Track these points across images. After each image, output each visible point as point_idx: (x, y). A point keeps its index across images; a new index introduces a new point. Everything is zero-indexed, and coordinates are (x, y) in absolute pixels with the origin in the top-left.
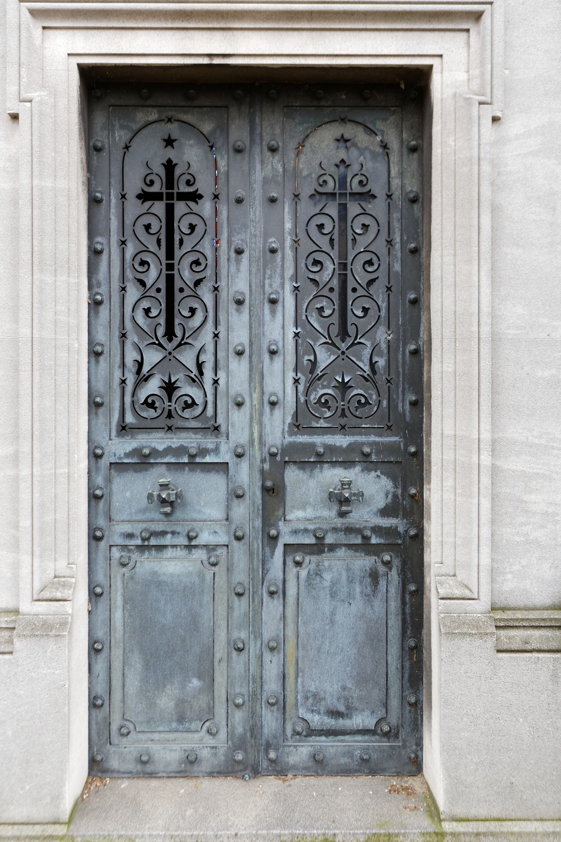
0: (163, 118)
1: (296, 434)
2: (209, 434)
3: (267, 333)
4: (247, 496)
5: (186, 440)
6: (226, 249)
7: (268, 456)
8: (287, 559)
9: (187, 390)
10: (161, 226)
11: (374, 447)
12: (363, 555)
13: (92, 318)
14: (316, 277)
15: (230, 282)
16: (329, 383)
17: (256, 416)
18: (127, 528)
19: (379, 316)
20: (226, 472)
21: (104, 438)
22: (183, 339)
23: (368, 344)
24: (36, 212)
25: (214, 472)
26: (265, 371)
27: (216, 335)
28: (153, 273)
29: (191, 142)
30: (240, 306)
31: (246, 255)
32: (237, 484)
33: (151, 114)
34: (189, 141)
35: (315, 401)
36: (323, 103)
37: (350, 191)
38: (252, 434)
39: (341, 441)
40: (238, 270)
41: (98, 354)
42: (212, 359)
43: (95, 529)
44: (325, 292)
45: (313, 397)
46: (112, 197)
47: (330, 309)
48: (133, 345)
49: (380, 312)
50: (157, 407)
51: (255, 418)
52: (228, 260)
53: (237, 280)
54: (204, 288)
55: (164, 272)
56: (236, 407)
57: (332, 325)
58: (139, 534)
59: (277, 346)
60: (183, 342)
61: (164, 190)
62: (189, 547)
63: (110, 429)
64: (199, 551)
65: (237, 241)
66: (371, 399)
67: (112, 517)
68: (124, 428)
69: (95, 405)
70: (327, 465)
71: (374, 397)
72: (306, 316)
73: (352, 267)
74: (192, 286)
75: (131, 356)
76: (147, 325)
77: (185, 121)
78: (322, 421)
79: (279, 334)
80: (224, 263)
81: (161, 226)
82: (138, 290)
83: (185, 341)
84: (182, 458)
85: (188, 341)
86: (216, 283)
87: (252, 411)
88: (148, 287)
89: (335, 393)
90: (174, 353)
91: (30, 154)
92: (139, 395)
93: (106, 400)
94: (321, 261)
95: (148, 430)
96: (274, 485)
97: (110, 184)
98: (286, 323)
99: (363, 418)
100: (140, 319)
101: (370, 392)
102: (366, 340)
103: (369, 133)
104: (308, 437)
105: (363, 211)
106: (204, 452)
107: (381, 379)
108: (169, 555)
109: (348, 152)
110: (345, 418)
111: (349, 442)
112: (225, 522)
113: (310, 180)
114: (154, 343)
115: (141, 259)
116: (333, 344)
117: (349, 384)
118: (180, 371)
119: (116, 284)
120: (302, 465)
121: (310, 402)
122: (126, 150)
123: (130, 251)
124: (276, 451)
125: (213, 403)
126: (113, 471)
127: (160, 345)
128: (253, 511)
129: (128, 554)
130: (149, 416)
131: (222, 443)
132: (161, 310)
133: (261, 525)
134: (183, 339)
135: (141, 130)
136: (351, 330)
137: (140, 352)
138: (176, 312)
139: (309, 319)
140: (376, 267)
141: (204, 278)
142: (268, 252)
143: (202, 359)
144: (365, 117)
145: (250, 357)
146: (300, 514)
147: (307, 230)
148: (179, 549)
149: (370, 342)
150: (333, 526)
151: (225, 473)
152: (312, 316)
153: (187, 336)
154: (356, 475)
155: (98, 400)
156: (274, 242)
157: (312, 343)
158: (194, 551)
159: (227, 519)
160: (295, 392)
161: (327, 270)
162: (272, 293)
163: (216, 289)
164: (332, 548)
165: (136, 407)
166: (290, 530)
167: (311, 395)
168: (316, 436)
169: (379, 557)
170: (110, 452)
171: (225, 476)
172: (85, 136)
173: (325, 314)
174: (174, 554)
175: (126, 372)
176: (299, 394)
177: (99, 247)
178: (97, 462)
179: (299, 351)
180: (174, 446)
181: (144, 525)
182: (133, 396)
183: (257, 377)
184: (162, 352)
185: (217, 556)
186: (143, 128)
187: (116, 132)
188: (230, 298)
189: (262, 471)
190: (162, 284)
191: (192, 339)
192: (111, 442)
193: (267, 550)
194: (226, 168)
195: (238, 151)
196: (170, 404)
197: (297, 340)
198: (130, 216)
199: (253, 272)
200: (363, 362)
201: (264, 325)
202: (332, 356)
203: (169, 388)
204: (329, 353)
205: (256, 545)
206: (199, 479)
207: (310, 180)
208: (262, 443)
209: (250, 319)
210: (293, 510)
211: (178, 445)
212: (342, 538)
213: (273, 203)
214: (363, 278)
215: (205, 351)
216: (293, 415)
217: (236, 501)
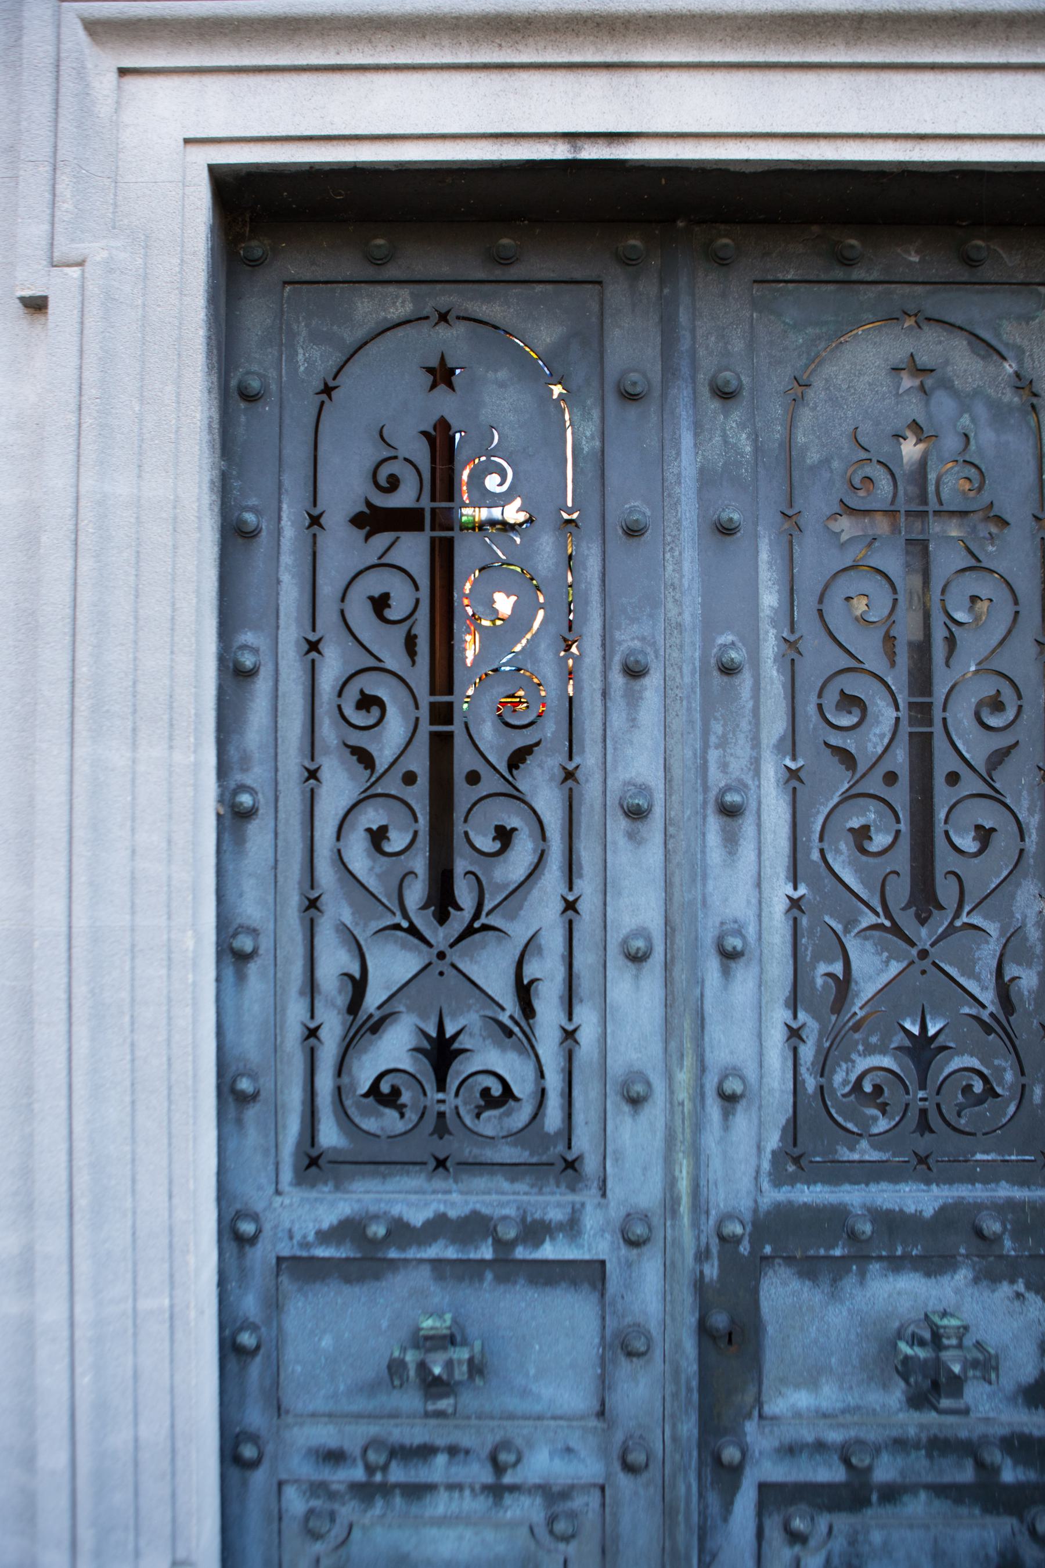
0: (425, 313)
1: (792, 1180)
2: (552, 1181)
3: (715, 900)
4: (658, 1354)
5: (487, 1198)
6: (598, 662)
7: (714, 1242)
8: (768, 1523)
9: (488, 1058)
10: (417, 601)
11: (1010, 1216)
12: (977, 1511)
13: (227, 856)
14: (849, 743)
15: (609, 758)
16: (886, 1038)
17: (684, 1134)
18: (325, 1435)
19: (1022, 851)
20: (600, 1287)
21: (260, 1188)
22: (477, 916)
23: (992, 928)
24: (86, 565)
25: (564, 1285)
26: (708, 1008)
27: (570, 906)
28: (395, 730)
29: (502, 374)
30: (639, 825)
31: (652, 682)
32: (629, 1320)
33: (394, 303)
34: (496, 371)
35: (847, 1089)
36: (857, 274)
37: (937, 508)
38: (671, 1183)
39: (919, 1199)
40: (633, 722)
41: (242, 958)
42: (560, 973)
43: (237, 1436)
44: (874, 784)
45: (841, 1078)
46: (285, 522)
47: (887, 832)
48: (337, 930)
49: (1022, 839)
50: (404, 1106)
51: (680, 1137)
52: (605, 694)
53: (629, 752)
54: (537, 771)
55: (426, 728)
56: (626, 1108)
57: (893, 876)
58: (357, 1452)
59: (744, 938)
60: (477, 925)
61: (426, 503)
62: (497, 1491)
63: (277, 1165)
64: (522, 1498)
65: (627, 639)
66: (1001, 1081)
67: (285, 1402)
68: (314, 1162)
69: (234, 1097)
70: (877, 1266)
71: (1009, 1076)
72: (822, 852)
73: (947, 714)
74: (503, 767)
75: (334, 962)
76: (379, 876)
77: (486, 319)
78: (864, 1144)
79: (749, 902)
80: (592, 702)
81: (417, 601)
82: (353, 777)
83: (483, 920)
84: (476, 1248)
85: (492, 921)
86: (571, 758)
87: (672, 1120)
88: (380, 768)
89: (900, 1065)
90: (453, 956)
91: (73, 406)
92: (355, 1070)
93: (266, 1084)
94: (862, 697)
95: (382, 1168)
96: (732, 1321)
97: (280, 488)
98: (767, 871)
99: (979, 1135)
100: (359, 857)
101: (996, 1062)
102: (986, 917)
103: (982, 353)
104: (827, 1188)
105: (973, 563)
106: (536, 1231)
107: (1026, 1026)
108: (441, 1510)
109: (927, 404)
110: (927, 1135)
111: (941, 1202)
112: (593, 1423)
113: (827, 475)
114: (397, 927)
115: (362, 692)
116: (896, 930)
117: (941, 1041)
118: (470, 1007)
119: (292, 762)
120: (809, 1268)
121: (833, 1091)
122: (324, 397)
123: (332, 668)
124: (739, 1230)
125: (562, 1094)
126: (284, 1279)
127: (413, 930)
128: (675, 1395)
129: (328, 1506)
130: (382, 1129)
131: (589, 1208)
132: (416, 833)
133: (696, 1432)
134: (477, 916)
135: (366, 343)
136: (946, 891)
137: (357, 952)
138: (458, 840)
139: (830, 861)
140: (1010, 714)
141: (537, 744)
142: (716, 673)
143: (530, 971)
144: (969, 307)
145: (667, 967)
146: (802, 1399)
147: (820, 611)
148: (467, 1493)
149: (998, 925)
150: (895, 1433)
151: (594, 1287)
152: (838, 851)
153: (487, 907)
154: (957, 1291)
155: (245, 1085)
156: (733, 643)
157: (838, 928)
158: (508, 1499)
159: (601, 1414)
160: (790, 1063)
161: (878, 722)
162: (728, 789)
163: (569, 775)
164: (891, 1494)
165: (348, 1103)
166: (777, 1444)
167: (833, 1072)
168: (847, 1187)
169: (1021, 1519)
170: (276, 1227)
171: (594, 1297)
172: (219, 362)
173: (874, 847)
174: (454, 1507)
175: (319, 1005)
176: (803, 1070)
177: (248, 661)
178: (241, 1255)
179: (801, 949)
180: (453, 1214)
181: (373, 1429)
182: (339, 1073)
183: (687, 1025)
184: (420, 952)
185: (572, 1515)
186: (373, 339)
187: (301, 351)
188: (612, 800)
189: (700, 1285)
190: (419, 762)
191: (504, 916)
192: (278, 1200)
193: (713, 1499)
194: (597, 443)
195: (629, 397)
196: (441, 1096)
197: (795, 919)
198: (333, 573)
199: (674, 727)
200: (977, 978)
201: (705, 877)
202: (893, 963)
203: (441, 1052)
204: (886, 954)
205: (682, 1489)
206: (523, 1305)
207: (827, 475)
208: (699, 1206)
209: (667, 859)
210: (784, 1390)
211: (466, 1210)
212: (921, 1467)
213: (729, 538)
214: (976, 747)
215: (540, 950)
216: (784, 1130)
217: (625, 1366)
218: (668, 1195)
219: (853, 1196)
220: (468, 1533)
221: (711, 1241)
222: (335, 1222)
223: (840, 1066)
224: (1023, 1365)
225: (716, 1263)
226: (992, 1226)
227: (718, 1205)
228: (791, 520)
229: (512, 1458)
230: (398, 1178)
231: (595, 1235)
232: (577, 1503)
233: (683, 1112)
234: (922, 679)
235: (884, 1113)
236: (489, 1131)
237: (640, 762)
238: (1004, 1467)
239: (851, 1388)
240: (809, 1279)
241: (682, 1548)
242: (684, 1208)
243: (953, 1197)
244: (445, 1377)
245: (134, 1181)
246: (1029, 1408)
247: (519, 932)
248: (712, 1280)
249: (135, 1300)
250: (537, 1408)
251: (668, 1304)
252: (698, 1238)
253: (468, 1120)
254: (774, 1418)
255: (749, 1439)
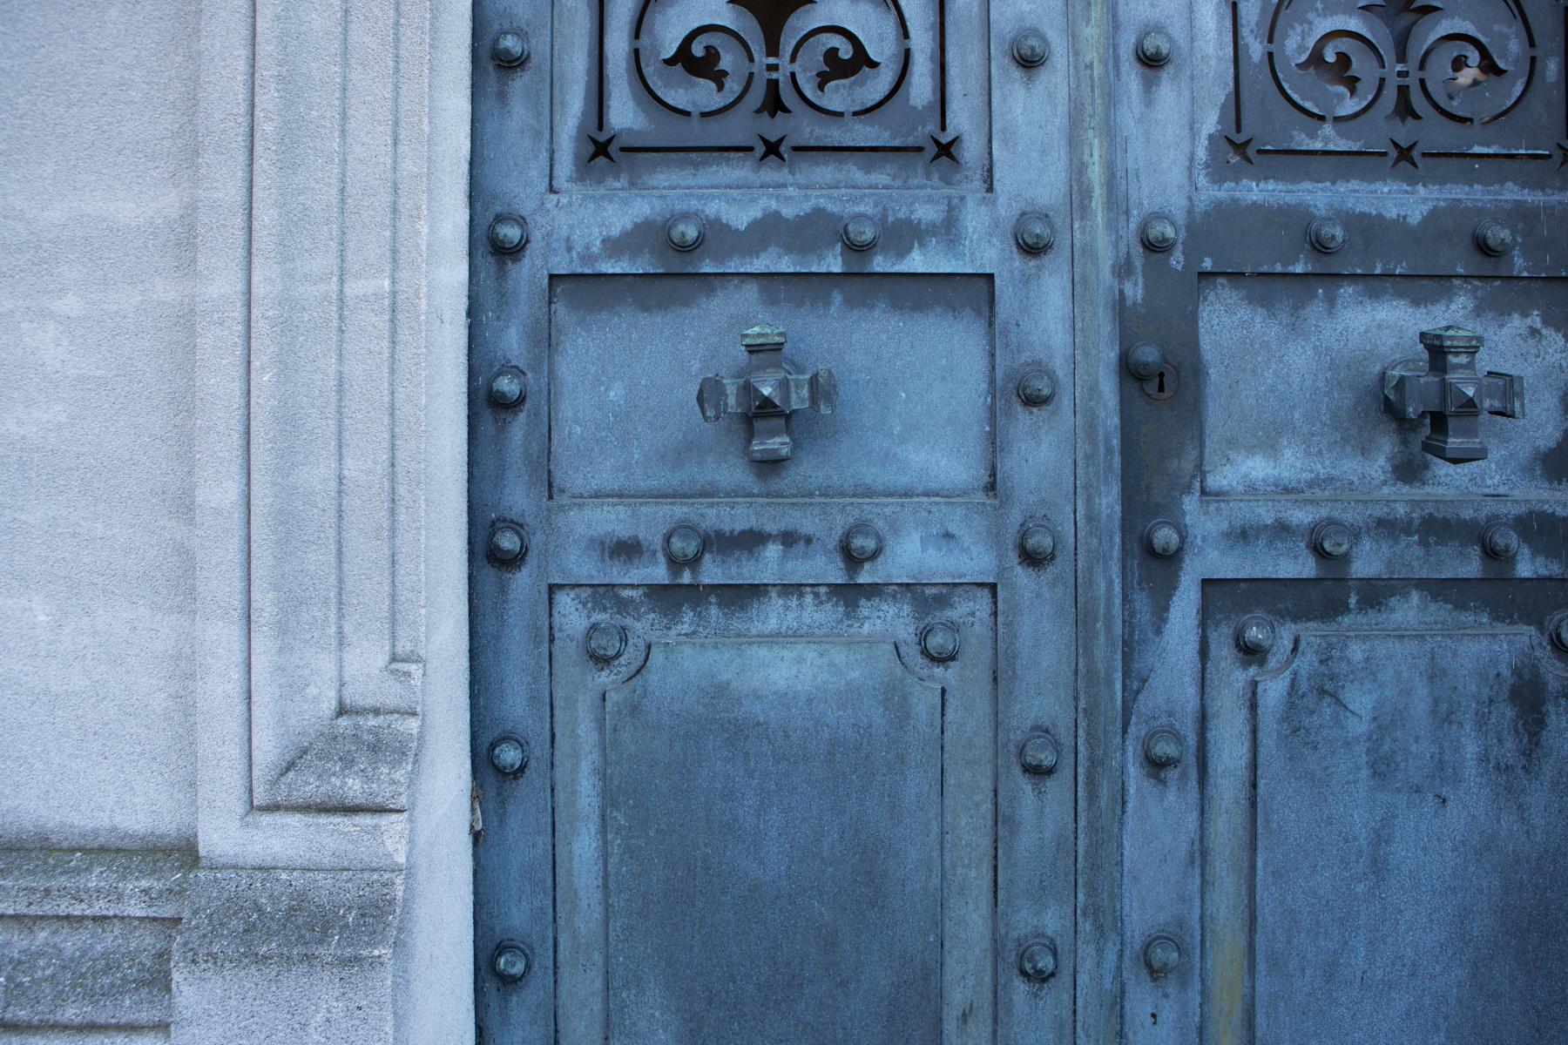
2: (921, 171)
4: (1066, 403)
5: (835, 192)
7: (1137, 250)
8: (1213, 636)
18: (613, 521)
32: (1026, 356)
38: (1078, 170)
39: (1403, 201)
43: (493, 523)
45: (1296, 44)
50: (724, 73)
51: (1089, 110)
56: (1017, 73)
58: (658, 543)
62: (849, 594)
64: (885, 607)
84: (821, 258)
92: (658, 28)
93: (539, 46)
95: (694, 155)
106: (904, 235)
108: (773, 624)
110: (1410, 121)
112: (980, 497)
120: (1262, 284)
124: (1170, 232)
126: (560, 308)
128: (1090, 457)
129: (618, 620)
131: (970, 204)
133: (1118, 508)
146: (1257, 468)
148: (809, 599)
150: (1379, 512)
151: (979, 313)
159: (991, 487)
160: (1228, 23)
164: (1376, 593)
165: (648, 71)
166: (1225, 526)
167: (1286, 35)
168: (1307, 185)
170: (549, 235)
171: (979, 327)
174: (791, 620)
176: (1245, 32)
178: (502, 274)
180: (788, 212)
181: (680, 511)
182: (637, 33)
185: (953, 627)
189: (1120, 307)
193: (1141, 601)
196: (772, 60)
205: (1103, 586)
206: (884, 337)
208: (1117, 204)
210: (1232, 455)
211: (807, 207)
212: (1413, 558)
217: (1024, 419)
218: (1075, 188)
220: (810, 654)
221: (1133, 251)
222: (629, 226)
223: (1293, 28)
224: (1540, 423)
225: (1140, 281)
227: (1141, 203)
229: (870, 544)
230: (714, 168)
231: (979, 239)
232: (960, 610)
233: (1091, 77)
235: (1353, 92)
236: (834, 104)
238: (1519, 558)
239: (1320, 452)
240: (1262, 306)
241: (1101, 668)
242: (1098, 193)
243: (1445, 200)
244: (777, 401)
245: (344, 116)
246: (1550, 481)
248: (1135, 303)
249: (342, 281)
250: (904, 480)
251: (1078, 333)
252: (1116, 246)
253: (809, 92)
254: (1221, 495)
255: (1188, 520)
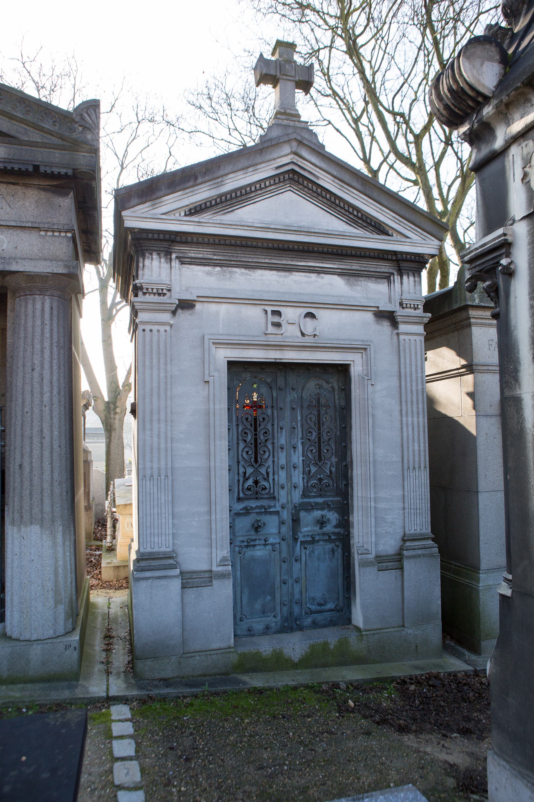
18: (241, 539)
28: (249, 437)
38: (288, 499)
39: (320, 500)
45: (310, 484)
62: (265, 545)
65: (281, 424)
75: (242, 470)
100: (245, 455)
120: (306, 510)
123: (240, 428)
136: (323, 458)
146: (306, 529)
164: (318, 541)
189: (292, 513)
190: (253, 442)
195: (280, 389)
203: (256, 482)
212: (321, 537)
217: (282, 526)
219: (312, 500)
226: (330, 503)
228: (302, 407)
234: (319, 429)
237: (283, 441)
247: (267, 465)
